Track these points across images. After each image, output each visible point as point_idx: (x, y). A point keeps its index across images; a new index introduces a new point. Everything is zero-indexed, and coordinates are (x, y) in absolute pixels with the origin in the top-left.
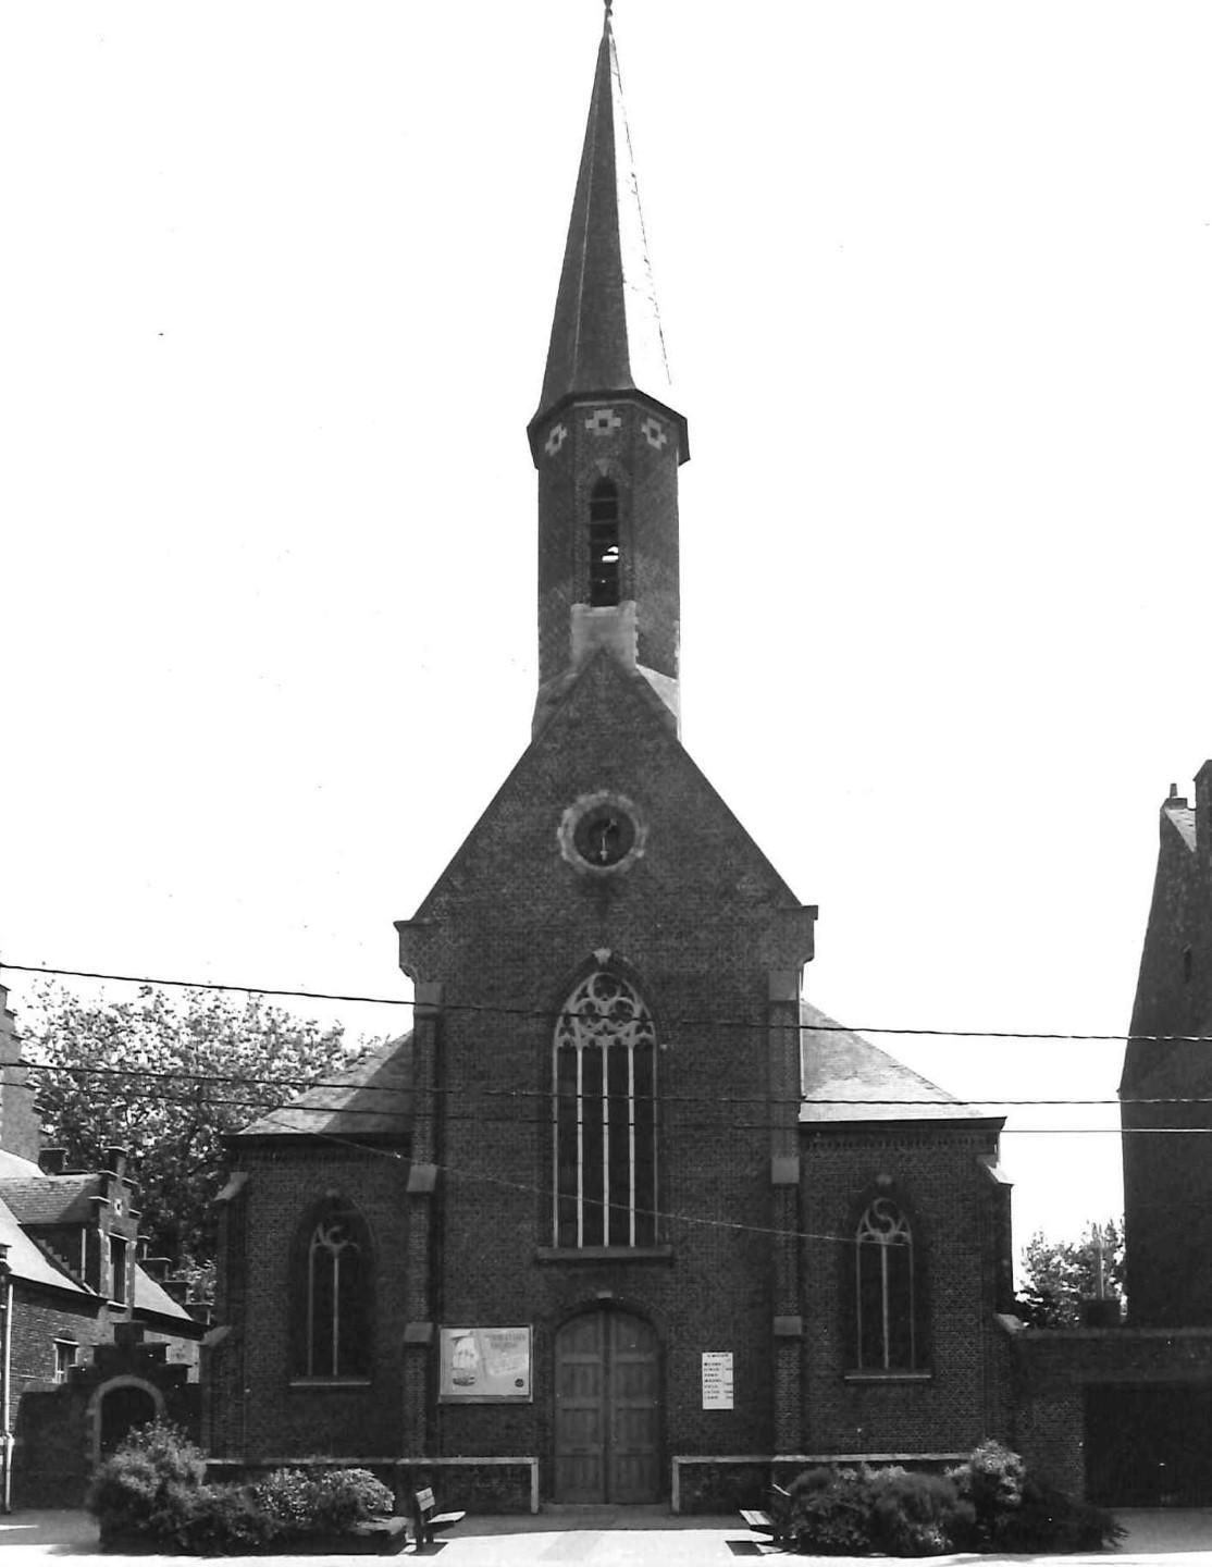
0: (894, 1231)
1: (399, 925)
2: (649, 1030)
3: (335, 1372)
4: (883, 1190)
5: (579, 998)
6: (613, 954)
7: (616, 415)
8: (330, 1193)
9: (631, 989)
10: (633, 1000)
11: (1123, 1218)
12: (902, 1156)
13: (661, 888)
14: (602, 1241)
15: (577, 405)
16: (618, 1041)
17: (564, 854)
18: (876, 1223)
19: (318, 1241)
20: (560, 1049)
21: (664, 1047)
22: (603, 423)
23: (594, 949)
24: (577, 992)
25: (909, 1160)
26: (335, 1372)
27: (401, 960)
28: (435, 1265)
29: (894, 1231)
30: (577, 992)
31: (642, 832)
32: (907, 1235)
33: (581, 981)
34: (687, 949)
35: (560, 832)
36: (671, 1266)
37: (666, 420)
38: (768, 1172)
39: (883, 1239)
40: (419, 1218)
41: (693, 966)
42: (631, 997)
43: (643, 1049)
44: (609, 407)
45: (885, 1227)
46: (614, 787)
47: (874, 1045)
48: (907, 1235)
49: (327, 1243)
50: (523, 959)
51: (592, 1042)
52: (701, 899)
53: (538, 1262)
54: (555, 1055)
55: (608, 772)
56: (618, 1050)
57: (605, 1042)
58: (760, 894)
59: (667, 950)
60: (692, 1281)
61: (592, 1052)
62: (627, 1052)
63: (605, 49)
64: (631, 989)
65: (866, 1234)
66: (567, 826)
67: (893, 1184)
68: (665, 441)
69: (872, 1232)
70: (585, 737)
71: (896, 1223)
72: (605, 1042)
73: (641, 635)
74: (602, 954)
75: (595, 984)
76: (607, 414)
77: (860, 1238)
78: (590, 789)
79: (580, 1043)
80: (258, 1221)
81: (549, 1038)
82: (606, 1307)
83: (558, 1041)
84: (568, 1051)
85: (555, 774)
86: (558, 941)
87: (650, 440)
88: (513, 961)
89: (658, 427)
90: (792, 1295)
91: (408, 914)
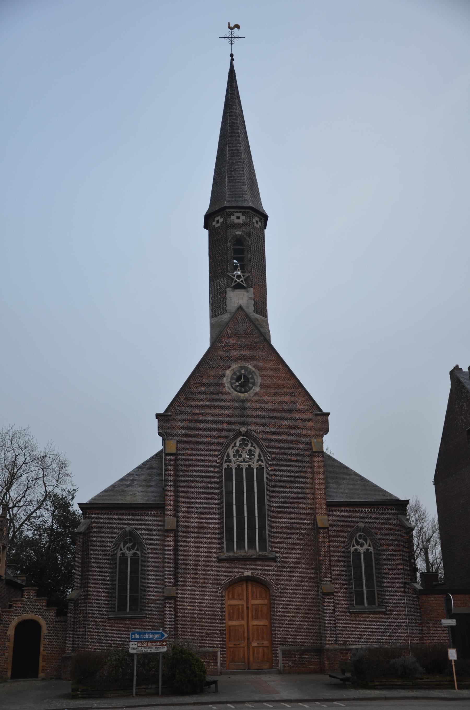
0: (366, 546)
1: (158, 416)
2: (262, 461)
3: (128, 610)
4: (360, 530)
5: (233, 447)
6: (247, 430)
7: (243, 215)
8: (128, 529)
9: (254, 445)
10: (255, 448)
11: (434, 480)
12: (368, 515)
13: (267, 404)
14: (126, 610)
15: (227, 210)
16: (249, 465)
17: (226, 388)
18: (358, 543)
19: (121, 550)
20: (225, 468)
21: (270, 469)
22: (238, 218)
23: (240, 428)
24: (233, 445)
25: (371, 517)
26: (128, 610)
27: (158, 430)
28: (176, 561)
29: (366, 546)
30: (233, 445)
31: (259, 380)
32: (371, 549)
33: (234, 440)
34: (278, 429)
35: (225, 379)
36: (276, 562)
37: (260, 217)
38: (315, 521)
39: (362, 550)
40: (170, 540)
41: (281, 436)
42: (254, 447)
43: (260, 469)
44: (241, 212)
45: (362, 545)
46: (247, 362)
47: (74, 499)
48: (371, 549)
49: (125, 550)
50: (210, 431)
51: (239, 466)
52: (283, 408)
53: (220, 560)
54: (223, 470)
55: (244, 355)
56: (250, 470)
57: (244, 466)
58: (306, 407)
59: (270, 429)
60: (284, 568)
61: (239, 469)
62: (232, 470)
63: (232, 74)
64: (254, 445)
65: (354, 548)
66: (228, 377)
67: (365, 526)
68: (261, 225)
69: (357, 547)
70: (235, 341)
71: (366, 543)
72: (244, 466)
73: (255, 301)
74: (243, 430)
75: (240, 441)
76: (240, 214)
77: (352, 549)
78: (235, 362)
79: (233, 466)
80: (95, 541)
81: (221, 464)
82: (247, 579)
83: (225, 466)
84: (229, 470)
85: (222, 355)
86: (225, 425)
87: (256, 225)
88: (206, 431)
89: (258, 219)
90: (328, 574)
91: (162, 411)
